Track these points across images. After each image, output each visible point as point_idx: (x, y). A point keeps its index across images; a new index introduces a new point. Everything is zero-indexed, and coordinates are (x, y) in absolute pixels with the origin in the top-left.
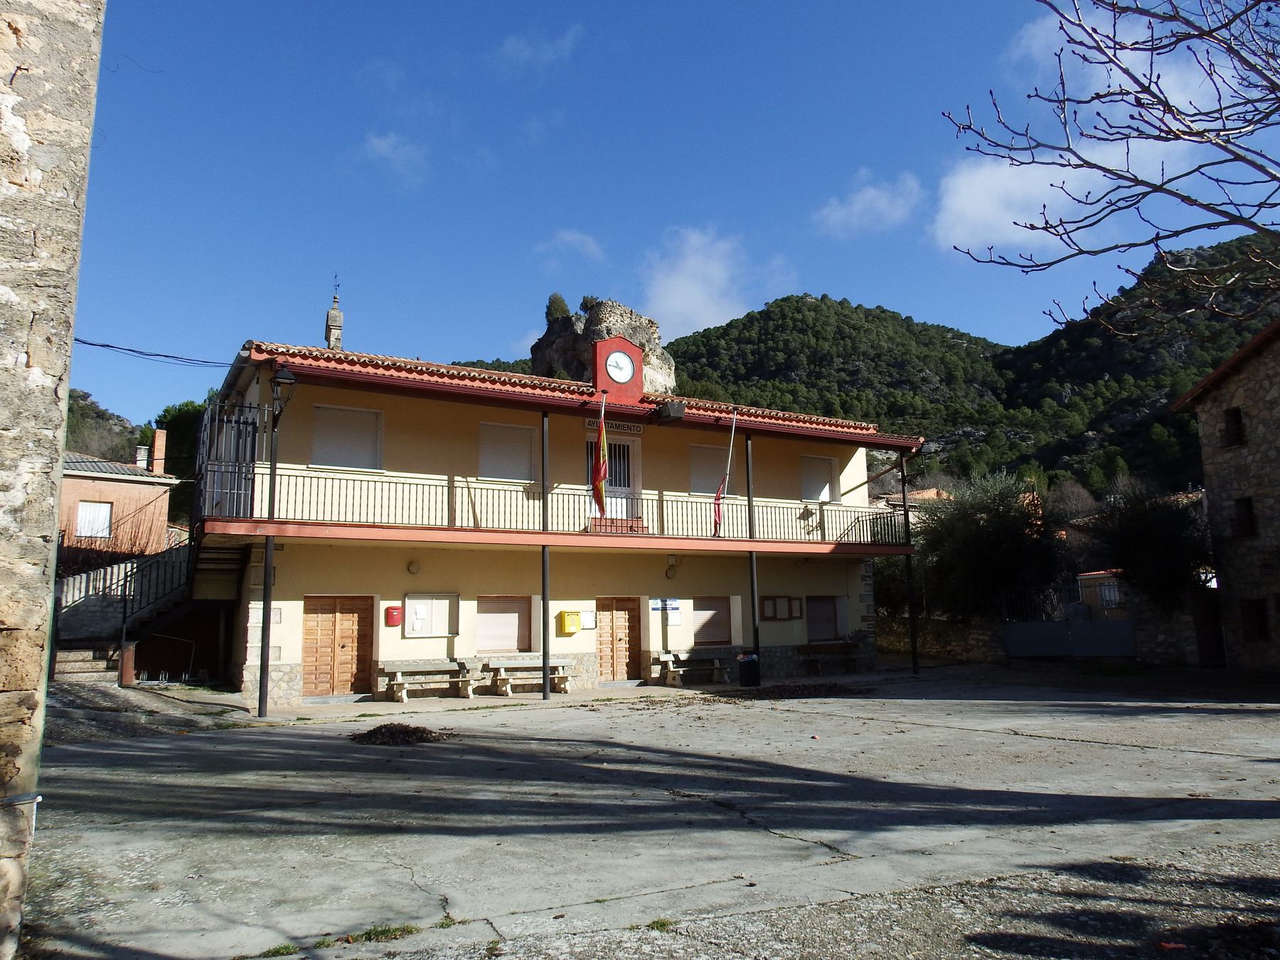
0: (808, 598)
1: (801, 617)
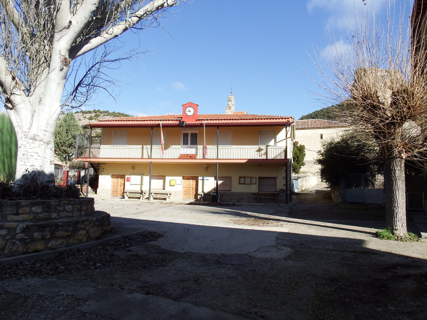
0: (259, 178)
1: (255, 184)
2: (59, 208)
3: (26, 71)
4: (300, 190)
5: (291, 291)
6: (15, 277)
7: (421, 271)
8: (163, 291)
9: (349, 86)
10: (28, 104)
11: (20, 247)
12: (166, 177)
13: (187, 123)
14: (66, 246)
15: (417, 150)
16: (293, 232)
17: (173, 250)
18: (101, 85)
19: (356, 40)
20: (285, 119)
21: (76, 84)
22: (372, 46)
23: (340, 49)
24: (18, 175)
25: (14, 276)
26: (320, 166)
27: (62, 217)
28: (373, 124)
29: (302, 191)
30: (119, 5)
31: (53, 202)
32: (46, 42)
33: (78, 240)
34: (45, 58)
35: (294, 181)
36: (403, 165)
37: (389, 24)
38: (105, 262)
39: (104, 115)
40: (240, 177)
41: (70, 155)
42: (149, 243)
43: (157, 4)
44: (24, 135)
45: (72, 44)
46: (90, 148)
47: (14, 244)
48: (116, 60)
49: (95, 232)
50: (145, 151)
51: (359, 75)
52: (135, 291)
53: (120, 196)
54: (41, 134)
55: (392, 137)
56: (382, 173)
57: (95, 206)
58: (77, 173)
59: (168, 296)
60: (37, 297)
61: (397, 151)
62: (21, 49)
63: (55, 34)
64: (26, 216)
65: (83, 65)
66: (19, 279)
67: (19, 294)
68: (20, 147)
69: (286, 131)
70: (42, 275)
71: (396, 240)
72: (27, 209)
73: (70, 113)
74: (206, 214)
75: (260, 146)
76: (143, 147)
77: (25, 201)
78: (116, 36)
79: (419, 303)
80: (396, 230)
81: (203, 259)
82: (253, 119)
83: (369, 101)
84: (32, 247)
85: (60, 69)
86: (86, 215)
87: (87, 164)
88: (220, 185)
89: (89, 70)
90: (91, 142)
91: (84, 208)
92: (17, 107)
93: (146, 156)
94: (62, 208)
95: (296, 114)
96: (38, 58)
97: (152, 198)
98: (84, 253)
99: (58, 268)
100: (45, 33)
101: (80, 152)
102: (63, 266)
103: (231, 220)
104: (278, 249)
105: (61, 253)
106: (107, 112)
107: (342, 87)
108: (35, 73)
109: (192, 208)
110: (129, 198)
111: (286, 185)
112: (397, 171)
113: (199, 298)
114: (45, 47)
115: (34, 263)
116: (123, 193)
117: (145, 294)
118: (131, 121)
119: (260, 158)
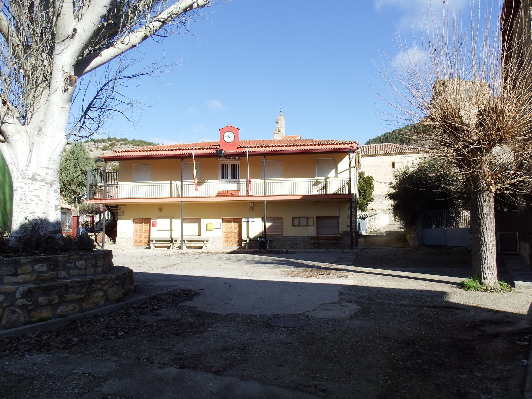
1: (313, 225)
2: (69, 265)
3: (20, 93)
4: (368, 232)
5: (358, 358)
6: (17, 353)
7: (514, 328)
8: (201, 364)
9: (426, 104)
10: (25, 134)
11: (22, 316)
12: (202, 220)
13: (226, 152)
14: (79, 312)
15: (508, 181)
16: (360, 285)
17: (212, 312)
18: (117, 108)
19: (432, 46)
20: (348, 144)
21: (85, 108)
22: (453, 54)
23: (414, 56)
24: (16, 225)
25: (16, 352)
26: (392, 202)
27: (73, 276)
28: (455, 151)
29: (371, 232)
30: (136, 6)
31: (61, 257)
32: (44, 55)
33: (93, 303)
34: (44, 76)
35: (361, 221)
36: (492, 200)
37: (473, 26)
38: (129, 330)
39: (121, 144)
40: (294, 218)
41: (80, 195)
42: (183, 304)
43: (184, 4)
44: (21, 175)
45: (78, 57)
46: (105, 187)
47: (14, 312)
48: (134, 76)
49: (114, 292)
50: (174, 187)
51: (439, 89)
52: (167, 364)
53: (145, 245)
54: (43, 173)
55: (479, 166)
56: (468, 209)
57: (114, 260)
58: (89, 219)
59: (208, 370)
60: (46, 378)
61: (484, 182)
62: (13, 65)
63: (56, 45)
64: (27, 277)
65: (93, 83)
66: (22, 356)
67: (22, 375)
68: (16, 190)
69: (350, 159)
70: (51, 350)
71: (484, 291)
72: (29, 268)
73: (78, 143)
74: (253, 265)
75: (317, 178)
76: (171, 183)
77: (26, 258)
78: (134, 46)
79: (510, 367)
80: (484, 278)
81: (250, 322)
82: (308, 145)
83: (450, 122)
84: (36, 315)
85: (64, 89)
86: (103, 272)
87: (101, 206)
88: (269, 227)
89: (101, 90)
90: (106, 180)
91: (100, 263)
92: (11, 139)
93: (175, 194)
94: (73, 264)
95: (360, 137)
96: (35, 77)
97: (184, 247)
98: (102, 320)
99: (70, 339)
100: (43, 44)
101: (92, 191)
102: (77, 337)
103: (284, 271)
104: (342, 306)
105: (74, 321)
106: (125, 140)
107: (417, 105)
108: (31, 96)
109: (236, 258)
110: (156, 247)
111: (351, 226)
112: (485, 207)
113: (246, 370)
114: (43, 61)
115: (40, 335)
116: (149, 241)
117: (180, 368)
118: (156, 151)
119: (318, 193)
